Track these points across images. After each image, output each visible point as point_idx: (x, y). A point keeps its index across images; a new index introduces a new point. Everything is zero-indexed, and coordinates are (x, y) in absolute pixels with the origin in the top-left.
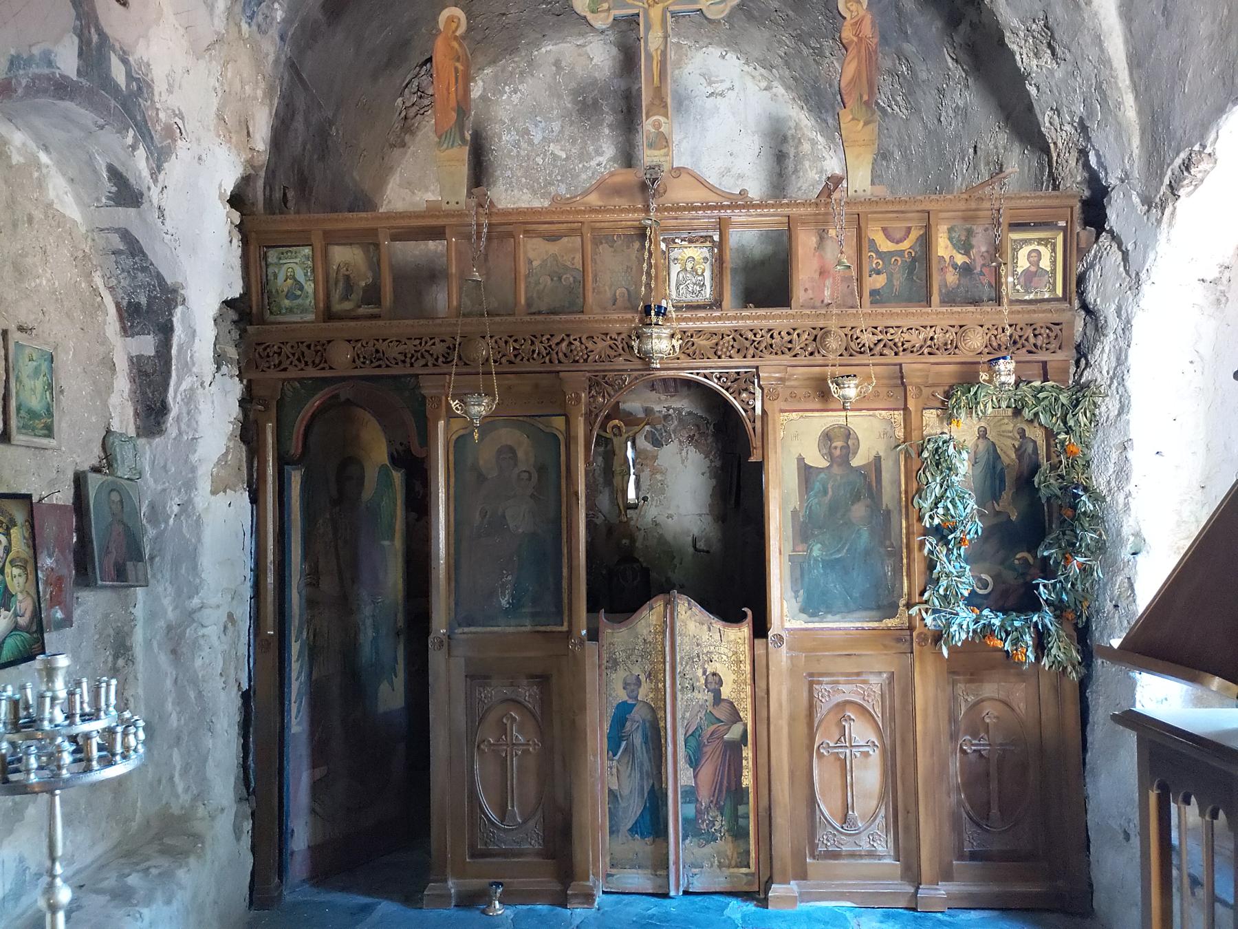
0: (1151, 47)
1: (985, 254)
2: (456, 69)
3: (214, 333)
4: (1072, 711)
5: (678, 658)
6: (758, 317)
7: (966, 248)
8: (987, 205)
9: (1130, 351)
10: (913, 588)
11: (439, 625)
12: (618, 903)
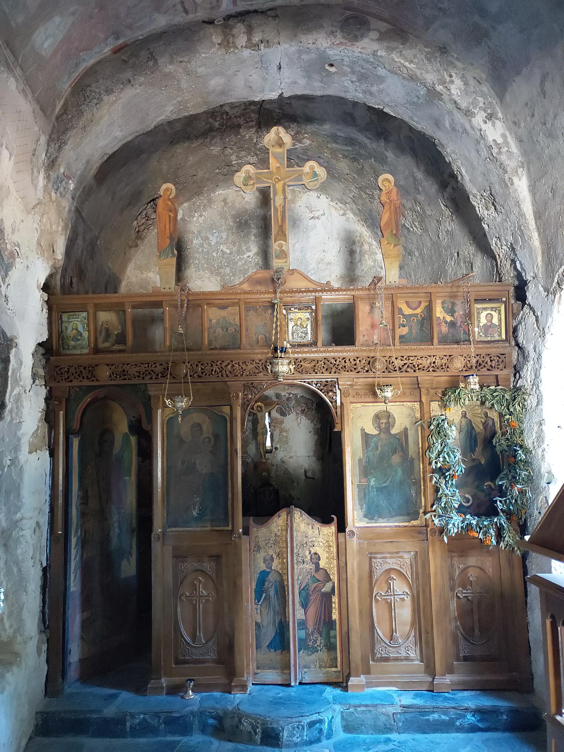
0: (545, 209)
1: (462, 316)
2: (170, 216)
3: (32, 362)
4: (518, 572)
5: (295, 545)
6: (337, 351)
7: (452, 312)
8: (461, 290)
9: (542, 371)
10: (427, 502)
11: (158, 528)
12: (260, 690)
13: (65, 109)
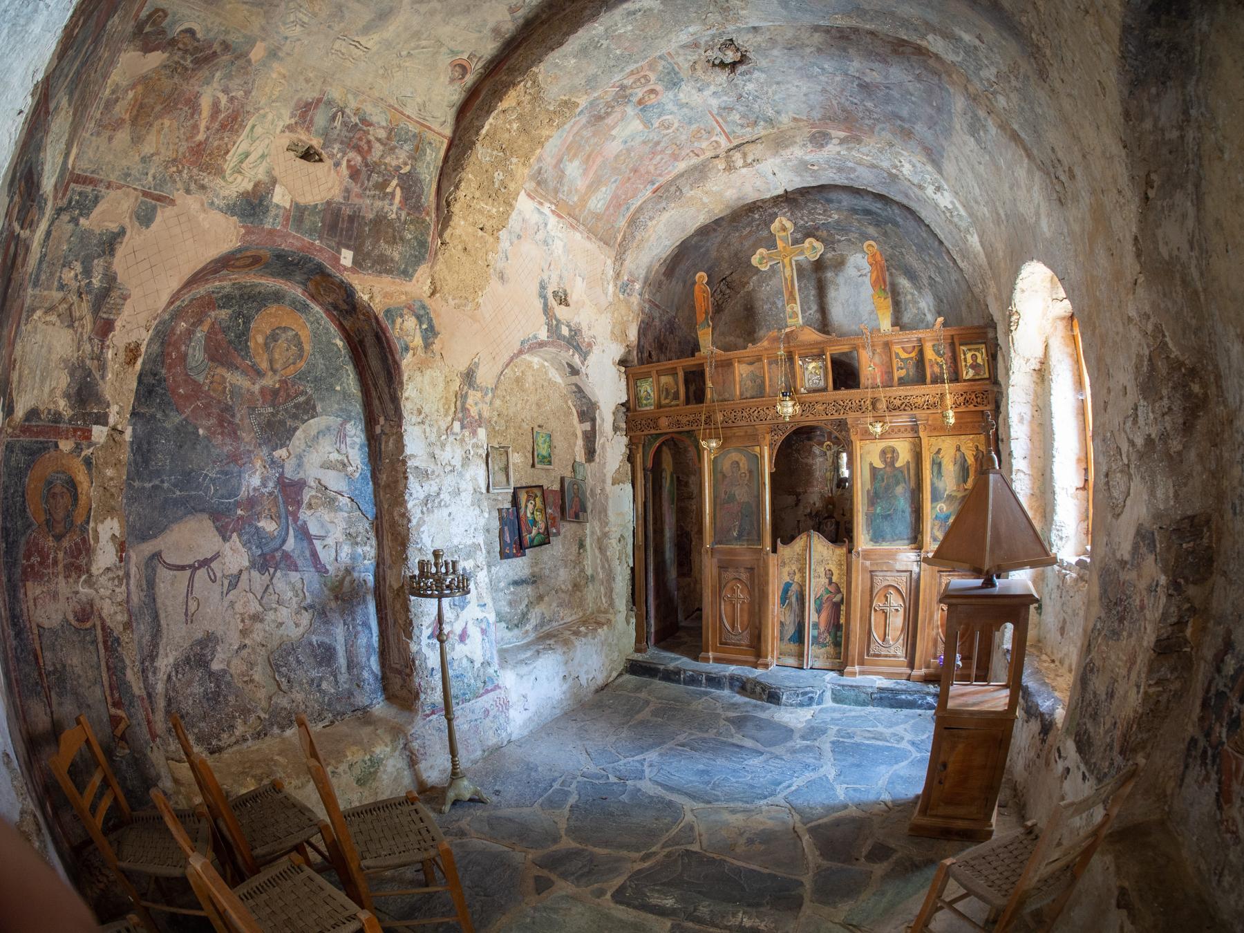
13: (624, 238)
